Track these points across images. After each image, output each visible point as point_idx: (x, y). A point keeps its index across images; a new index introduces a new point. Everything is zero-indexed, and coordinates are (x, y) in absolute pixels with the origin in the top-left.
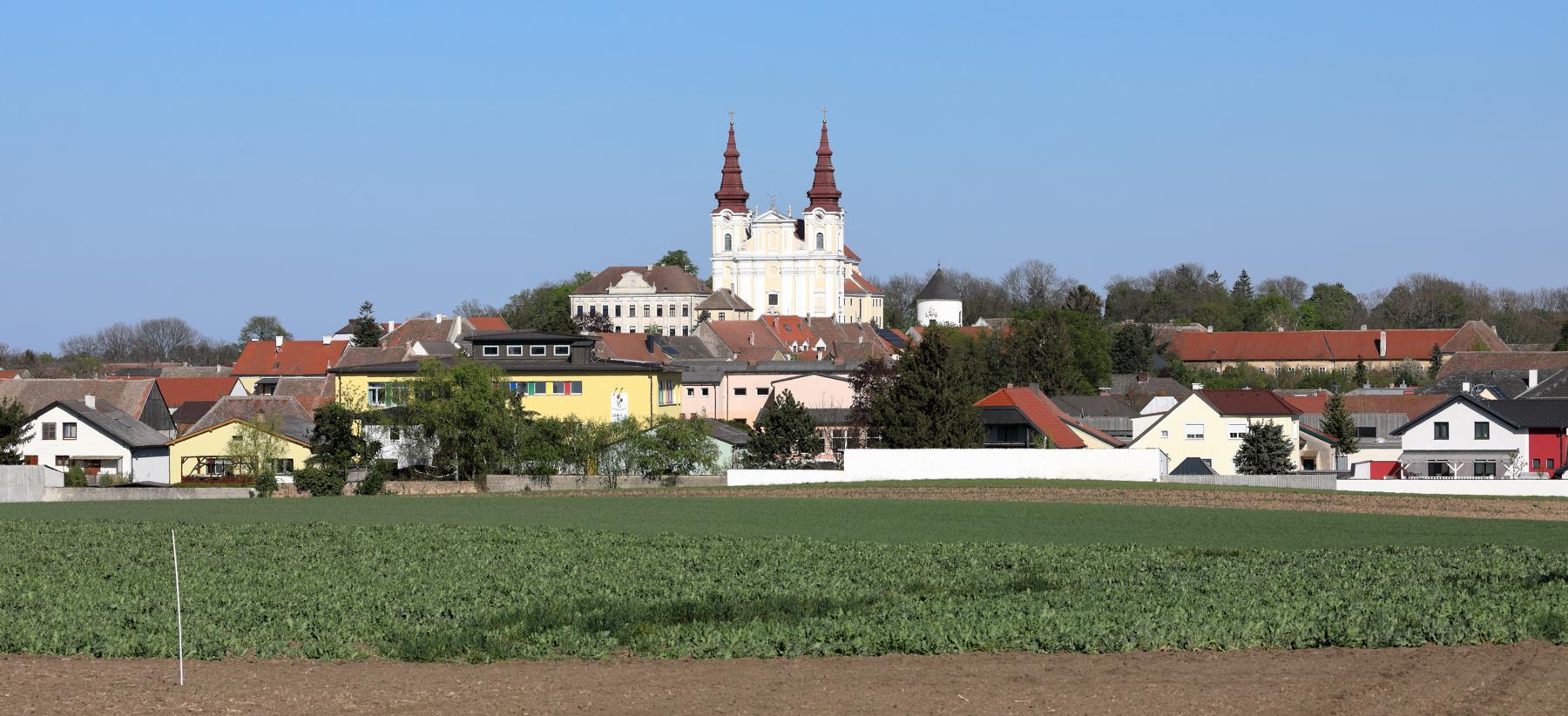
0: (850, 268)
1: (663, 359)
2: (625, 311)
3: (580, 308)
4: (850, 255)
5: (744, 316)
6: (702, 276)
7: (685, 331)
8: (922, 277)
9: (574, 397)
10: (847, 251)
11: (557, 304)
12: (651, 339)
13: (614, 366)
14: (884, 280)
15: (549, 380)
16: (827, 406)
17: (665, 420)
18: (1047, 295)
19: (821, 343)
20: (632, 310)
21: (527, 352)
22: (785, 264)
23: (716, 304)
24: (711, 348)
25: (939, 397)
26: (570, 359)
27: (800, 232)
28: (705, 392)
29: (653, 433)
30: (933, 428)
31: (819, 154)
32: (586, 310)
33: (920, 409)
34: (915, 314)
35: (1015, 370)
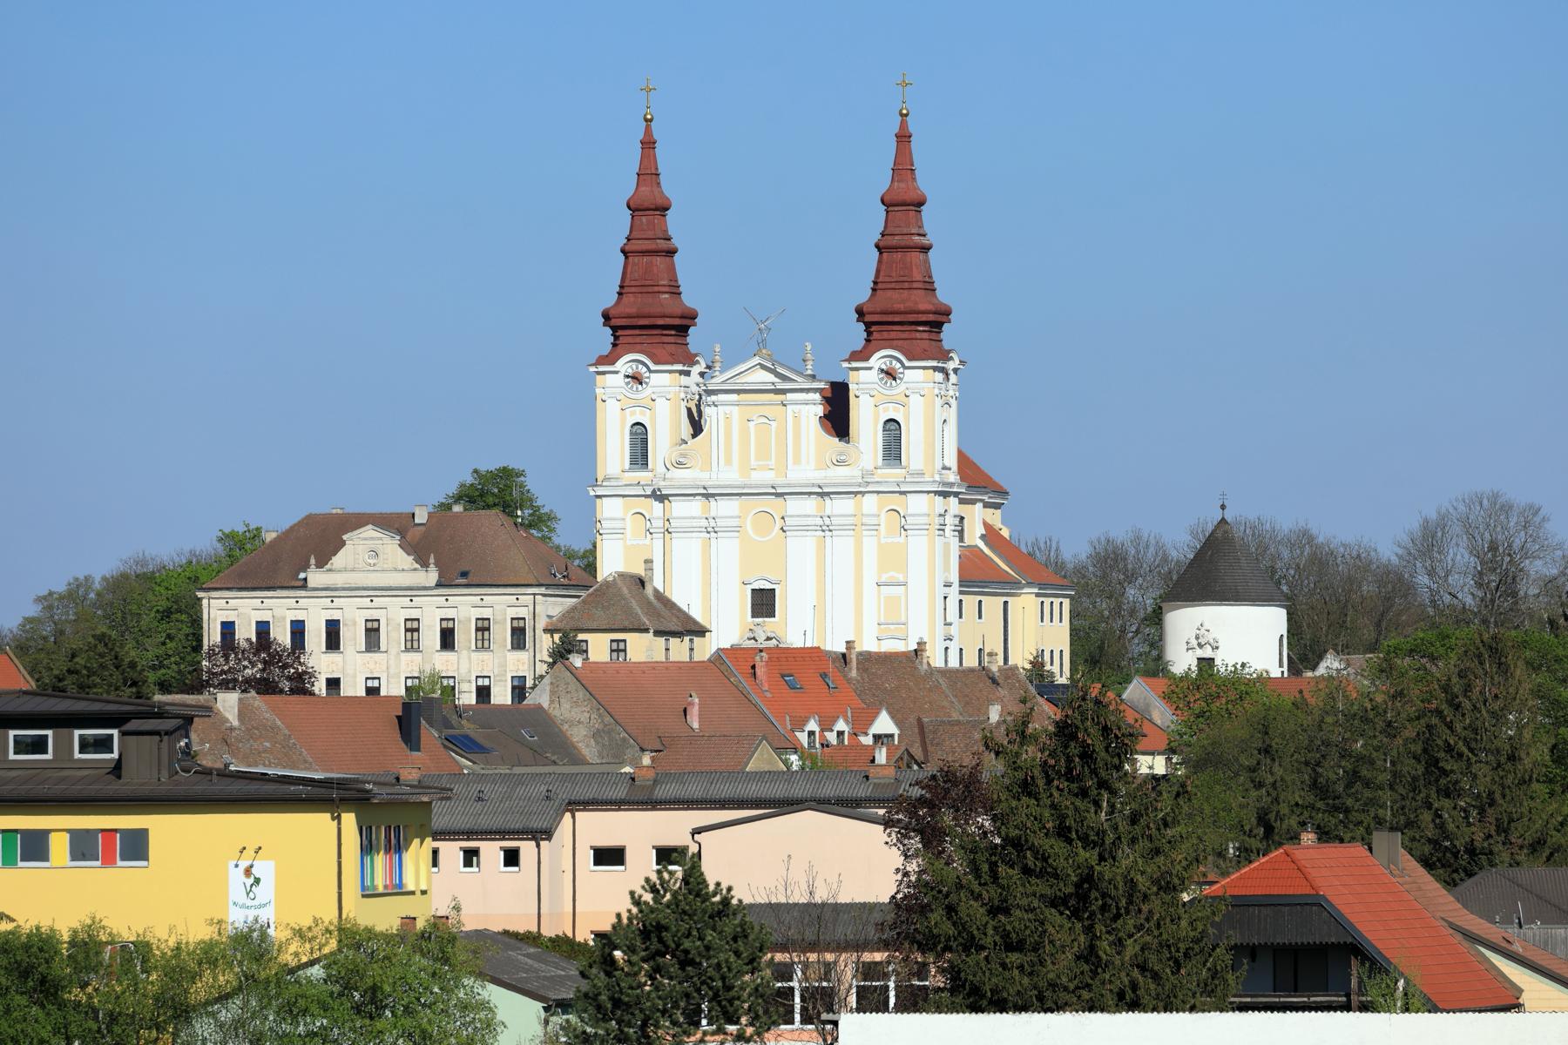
0: (977, 517)
1: (415, 772)
2: (353, 636)
3: (228, 628)
4: (975, 480)
5: (679, 650)
6: (566, 536)
7: (519, 690)
8: (1178, 538)
9: (125, 873)
10: (966, 464)
11: (166, 614)
12: (417, 713)
13: (236, 788)
14: (1076, 549)
15: (59, 826)
16: (800, 897)
17: (351, 937)
18: (1529, 589)
19: (884, 724)
20: (372, 634)
21: (64, 748)
22: (795, 506)
23: (601, 617)
24: (580, 736)
25: (1105, 870)
26: (117, 768)
27: (837, 418)
28: (512, 858)
29: (317, 972)
30: (1089, 955)
31: (635, 208)
32: (246, 633)
33: (1053, 903)
34: (1157, 643)
35: (1387, 797)
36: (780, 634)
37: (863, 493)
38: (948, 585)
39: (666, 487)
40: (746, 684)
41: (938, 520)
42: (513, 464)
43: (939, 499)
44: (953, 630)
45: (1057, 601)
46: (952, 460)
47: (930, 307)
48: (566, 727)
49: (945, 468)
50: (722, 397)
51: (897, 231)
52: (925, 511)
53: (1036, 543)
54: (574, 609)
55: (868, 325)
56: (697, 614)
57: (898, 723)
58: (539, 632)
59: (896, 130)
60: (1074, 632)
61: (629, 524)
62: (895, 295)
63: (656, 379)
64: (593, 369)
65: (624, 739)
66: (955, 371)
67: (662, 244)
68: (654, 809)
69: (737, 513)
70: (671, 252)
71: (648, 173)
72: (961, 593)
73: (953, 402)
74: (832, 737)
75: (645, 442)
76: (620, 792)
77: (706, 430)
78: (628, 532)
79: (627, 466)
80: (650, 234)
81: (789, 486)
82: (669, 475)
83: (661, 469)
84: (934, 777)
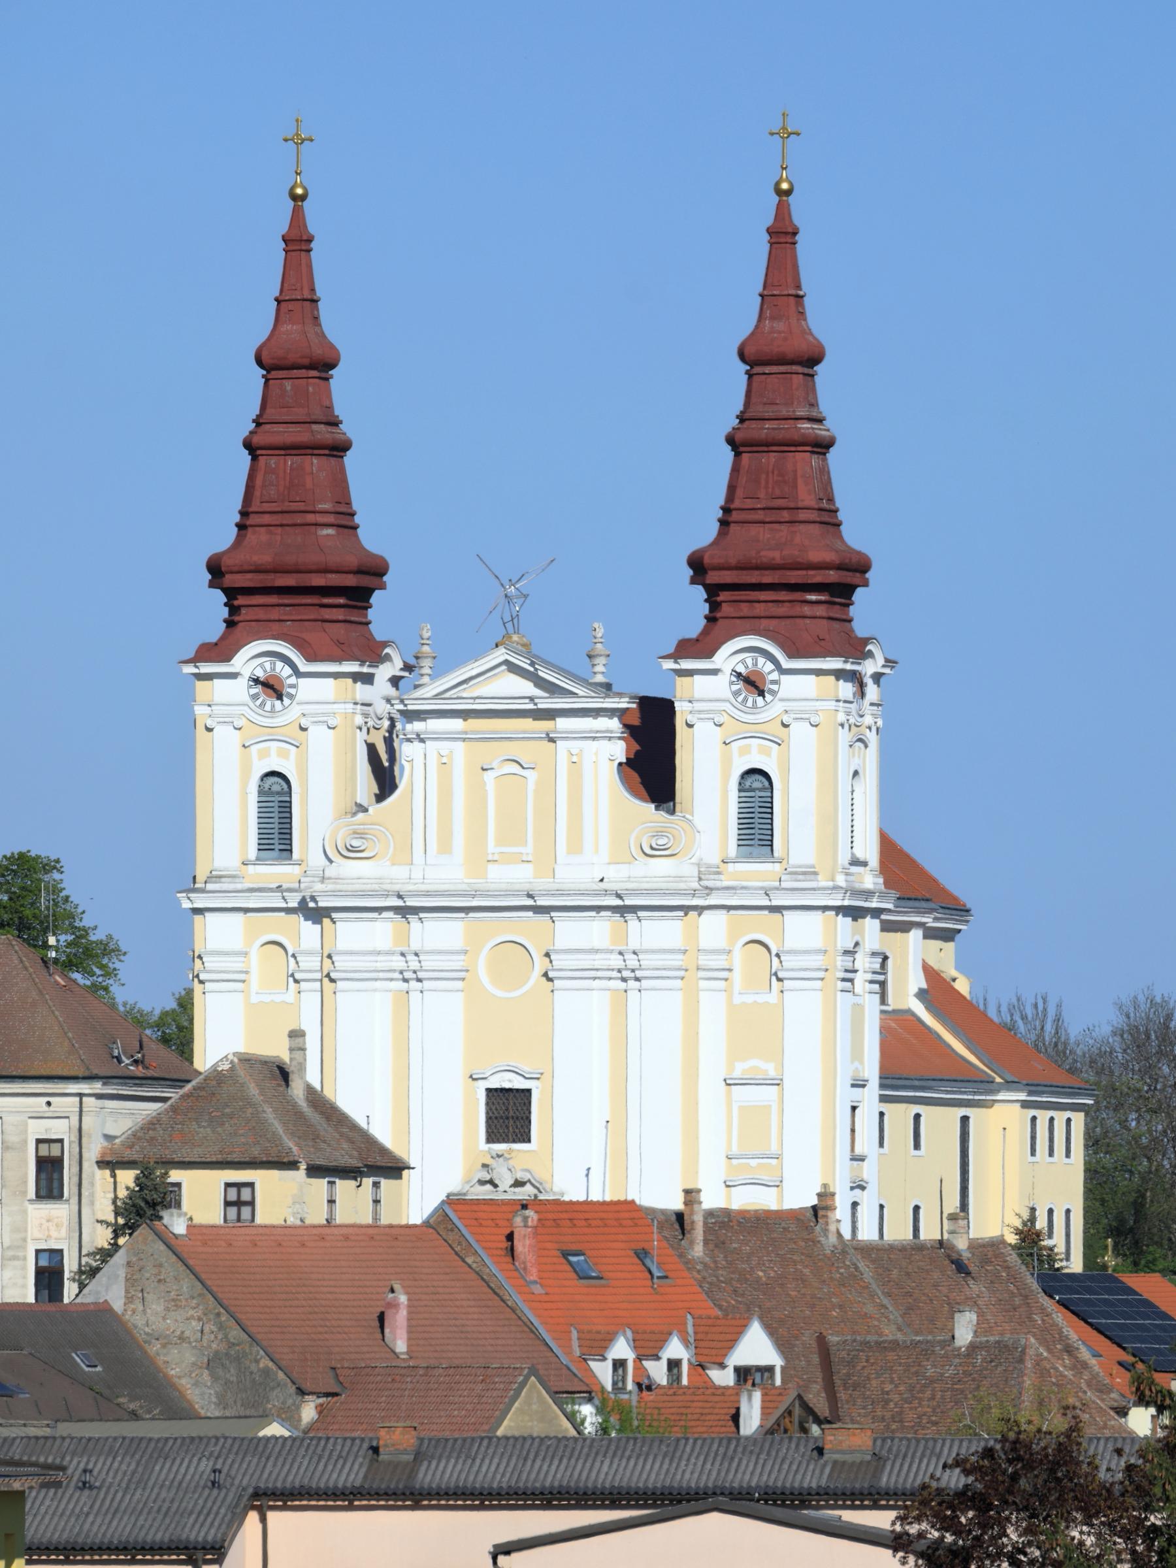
0: (913, 954)
4: (911, 888)
5: (353, 1202)
6: (138, 988)
10: (895, 860)
14: (1092, 1018)
19: (756, 1347)
22: (571, 932)
27: (652, 763)
36: (540, 1174)
37: (700, 909)
38: (859, 1084)
39: (327, 894)
40: (494, 1268)
41: (841, 962)
42: (38, 849)
43: (844, 922)
44: (868, 1171)
45: (1060, 1117)
46: (869, 850)
47: (830, 557)
48: (154, 1348)
49: (856, 862)
50: (434, 724)
51: (769, 412)
52: (818, 943)
53: (1017, 1006)
54: (152, 1124)
55: (713, 592)
56: (383, 1133)
57: (782, 1344)
58: (89, 1166)
59: (284, 228)
60: (1093, 1174)
61: (738, 959)
62: (763, 533)
63: (307, 689)
64: (189, 669)
65: (266, 1372)
66: (877, 677)
67: (322, 433)
68: (417, 1506)
69: (459, 945)
70: (340, 448)
71: (297, 299)
72: (884, 1099)
73: (872, 737)
74: (658, 1371)
75: (286, 809)
76: (352, 1474)
77: (402, 786)
78: (254, 979)
79: (252, 853)
80: (300, 413)
81: (561, 893)
82: (331, 871)
83: (316, 860)
84: (988, 1453)
